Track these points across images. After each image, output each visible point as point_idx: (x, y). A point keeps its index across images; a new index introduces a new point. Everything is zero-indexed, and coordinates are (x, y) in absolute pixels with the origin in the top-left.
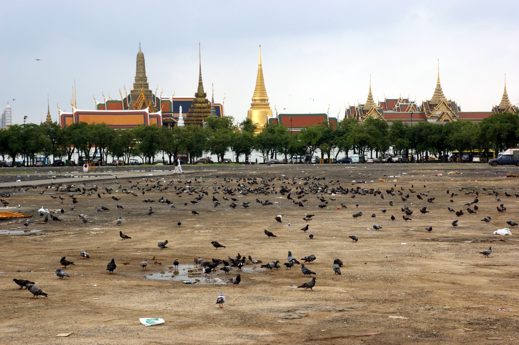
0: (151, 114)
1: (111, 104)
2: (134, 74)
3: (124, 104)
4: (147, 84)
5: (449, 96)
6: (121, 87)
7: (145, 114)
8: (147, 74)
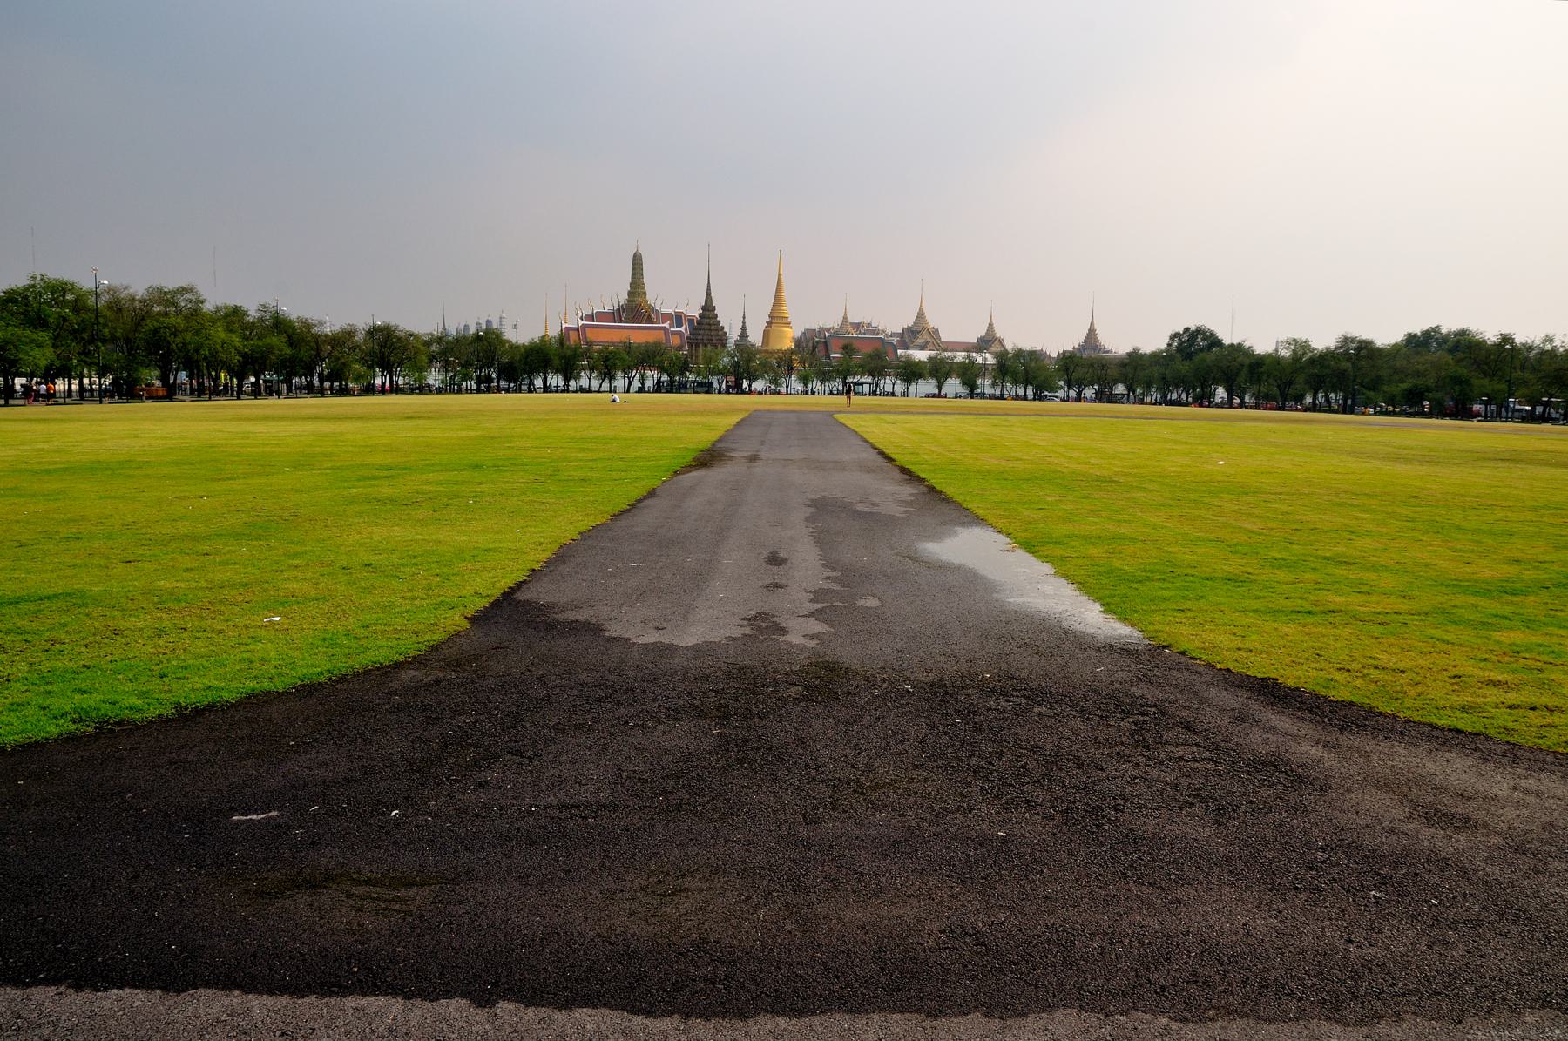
1: (601, 316)
3: (616, 315)
5: (932, 321)
6: (615, 295)
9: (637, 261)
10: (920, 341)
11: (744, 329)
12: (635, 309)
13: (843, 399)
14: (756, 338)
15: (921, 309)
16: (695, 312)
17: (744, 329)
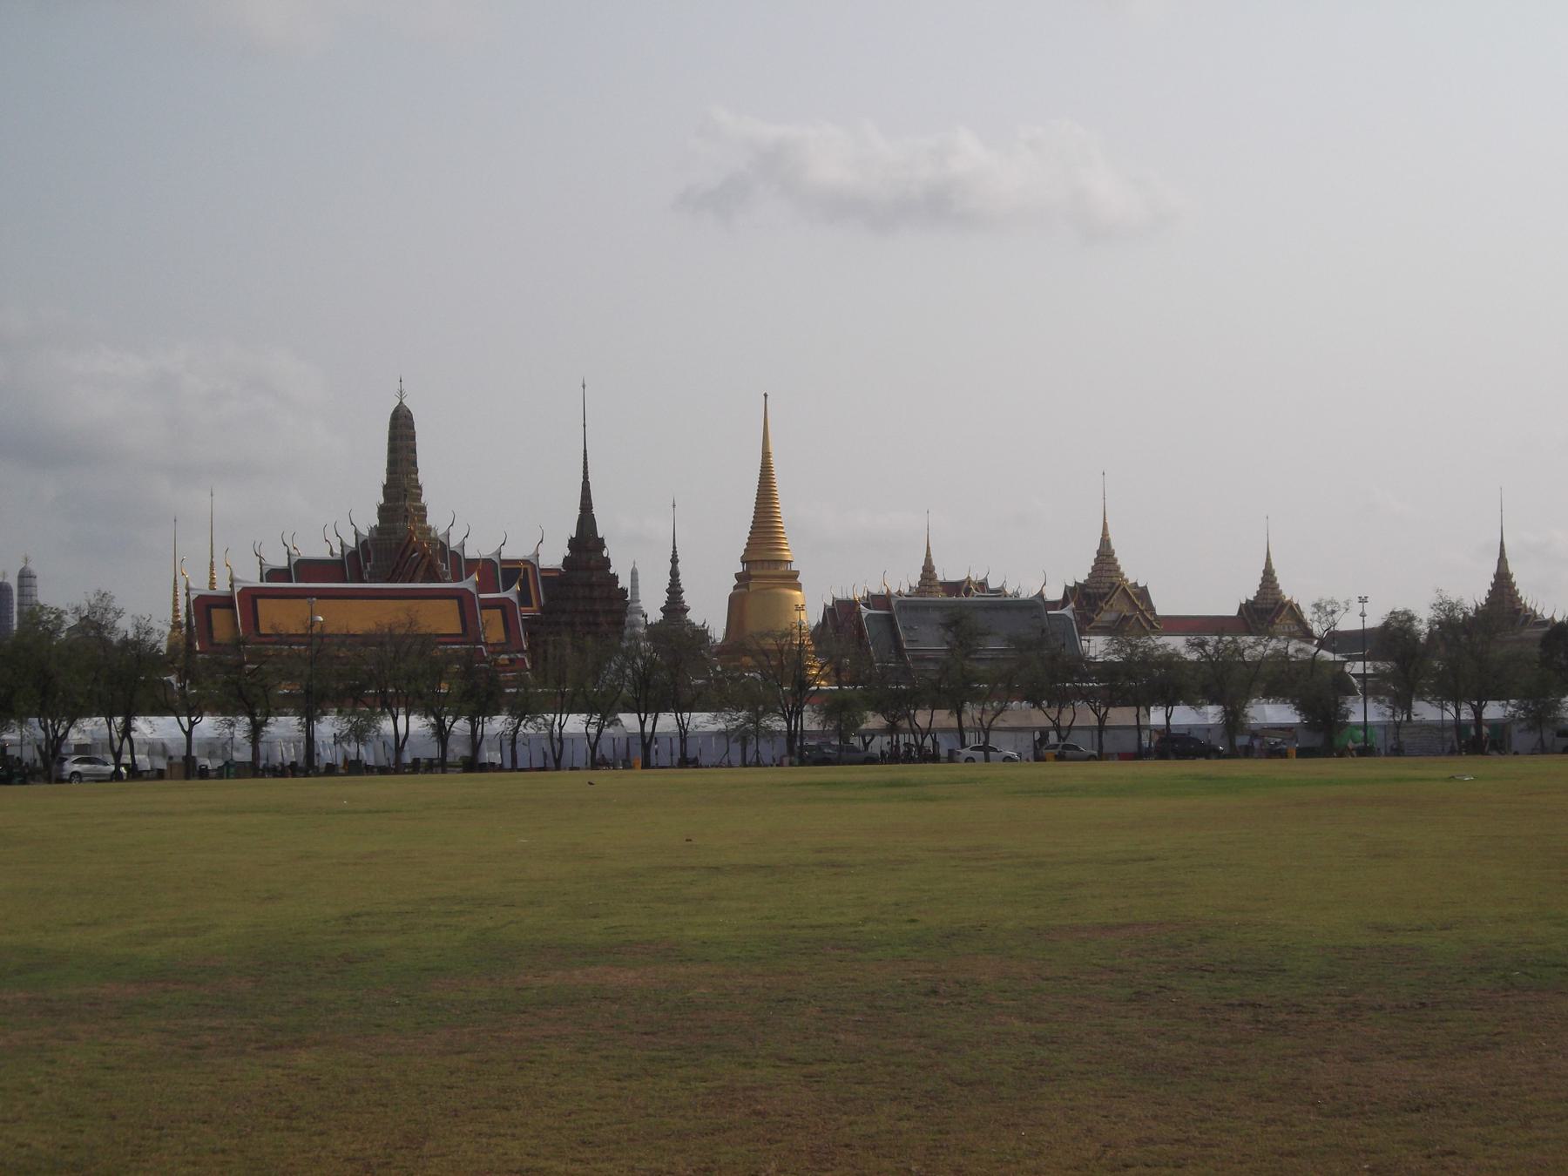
0: (482, 596)
1: (307, 568)
2: (382, 477)
4: (423, 509)
6: (344, 511)
7: (461, 597)
8: (422, 477)
9: (402, 429)
10: (1106, 617)
11: (675, 590)
12: (399, 542)
14: (709, 611)
15: (1105, 541)
16: (553, 556)
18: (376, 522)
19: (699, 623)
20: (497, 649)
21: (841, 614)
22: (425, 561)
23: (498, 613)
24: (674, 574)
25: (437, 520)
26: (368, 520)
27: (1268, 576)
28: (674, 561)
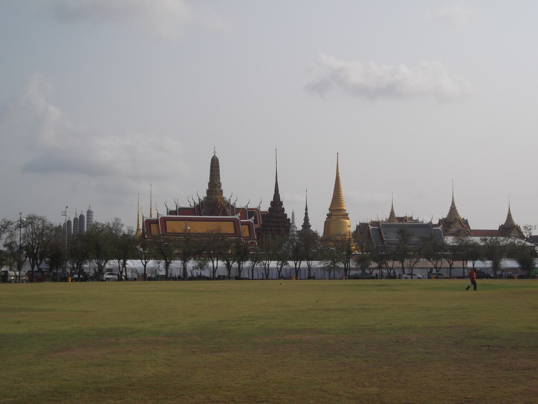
1: (182, 211)
6: (195, 192)
7: (234, 221)
9: (215, 164)
10: (453, 230)
11: (306, 219)
12: (214, 202)
13: (471, 292)
14: (318, 227)
15: (453, 204)
16: (265, 207)
17: (306, 219)
18: (206, 195)
19: (314, 230)
20: (246, 239)
21: (362, 228)
22: (222, 209)
23: (247, 226)
24: (306, 214)
25: (226, 195)
26: (203, 194)
27: (509, 216)
28: (306, 209)
